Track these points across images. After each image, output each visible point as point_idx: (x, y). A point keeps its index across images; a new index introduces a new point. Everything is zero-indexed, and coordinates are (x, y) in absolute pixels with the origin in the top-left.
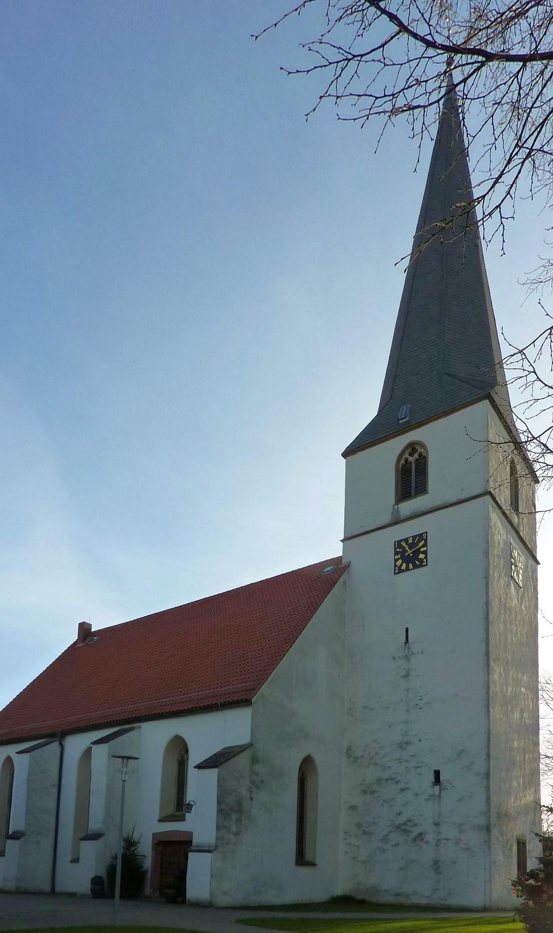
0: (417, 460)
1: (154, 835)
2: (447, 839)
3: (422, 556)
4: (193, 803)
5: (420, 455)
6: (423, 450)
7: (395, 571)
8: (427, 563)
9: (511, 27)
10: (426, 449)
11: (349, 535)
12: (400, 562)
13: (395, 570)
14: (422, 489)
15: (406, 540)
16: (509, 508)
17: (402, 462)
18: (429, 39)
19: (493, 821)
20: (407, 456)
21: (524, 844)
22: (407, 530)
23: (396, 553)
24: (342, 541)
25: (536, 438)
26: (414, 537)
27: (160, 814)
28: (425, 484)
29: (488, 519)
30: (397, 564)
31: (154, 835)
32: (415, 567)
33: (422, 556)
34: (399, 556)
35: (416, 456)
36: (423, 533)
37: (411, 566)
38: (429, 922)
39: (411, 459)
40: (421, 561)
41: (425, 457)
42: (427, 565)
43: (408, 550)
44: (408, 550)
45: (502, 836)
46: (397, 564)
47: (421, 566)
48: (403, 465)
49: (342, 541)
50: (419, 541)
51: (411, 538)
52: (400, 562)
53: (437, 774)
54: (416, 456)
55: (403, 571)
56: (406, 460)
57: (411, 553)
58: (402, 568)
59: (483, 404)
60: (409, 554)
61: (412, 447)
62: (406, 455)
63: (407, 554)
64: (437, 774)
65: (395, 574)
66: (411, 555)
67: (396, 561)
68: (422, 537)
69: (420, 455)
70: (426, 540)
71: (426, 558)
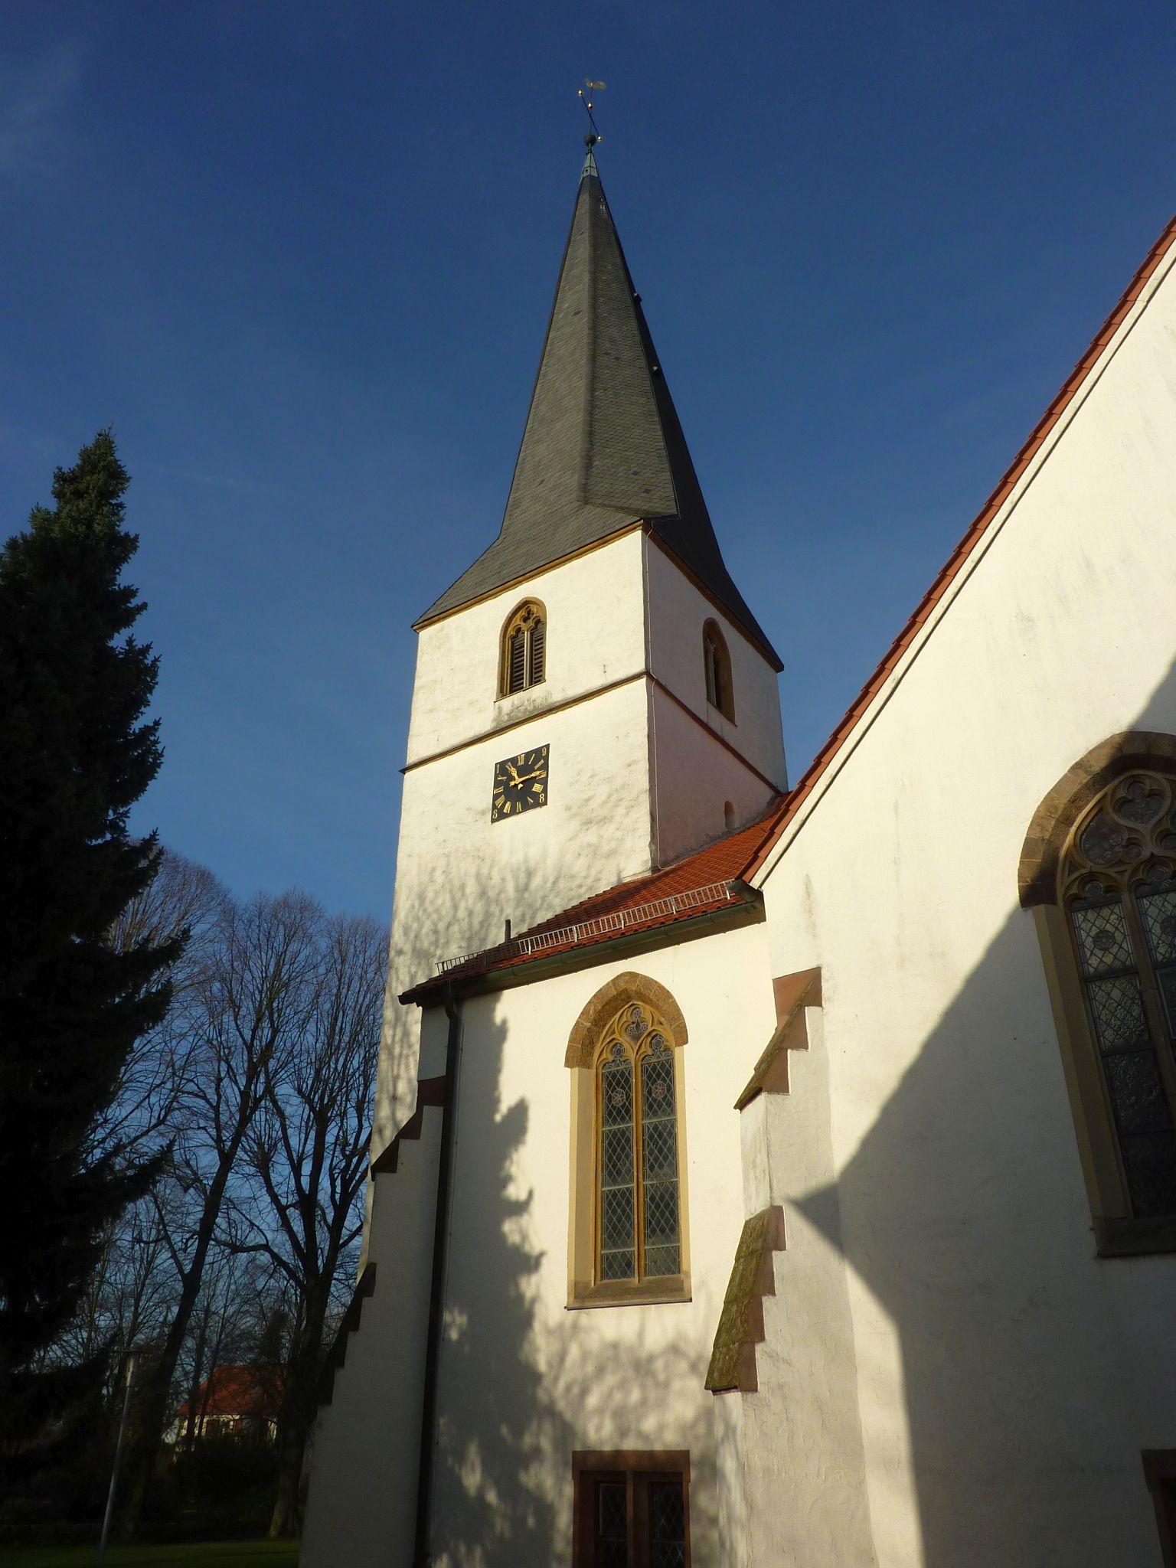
3: (537, 788)
9: (359, 1078)
12: (502, 798)
14: (537, 676)
15: (514, 761)
18: (346, 1223)
19: (206, 1273)
22: (517, 743)
23: (497, 785)
25: (1100, 988)
26: (528, 755)
28: (541, 671)
30: (497, 803)
32: (526, 807)
33: (537, 788)
34: (501, 789)
37: (519, 805)
38: (1083, 829)
40: (536, 795)
43: (516, 777)
44: (516, 777)
47: (538, 804)
50: (535, 762)
52: (502, 798)
57: (521, 783)
58: (505, 811)
59: (402, 1164)
60: (516, 785)
63: (512, 783)
66: (520, 786)
67: (496, 797)
68: (539, 757)
70: (546, 758)
71: (545, 791)
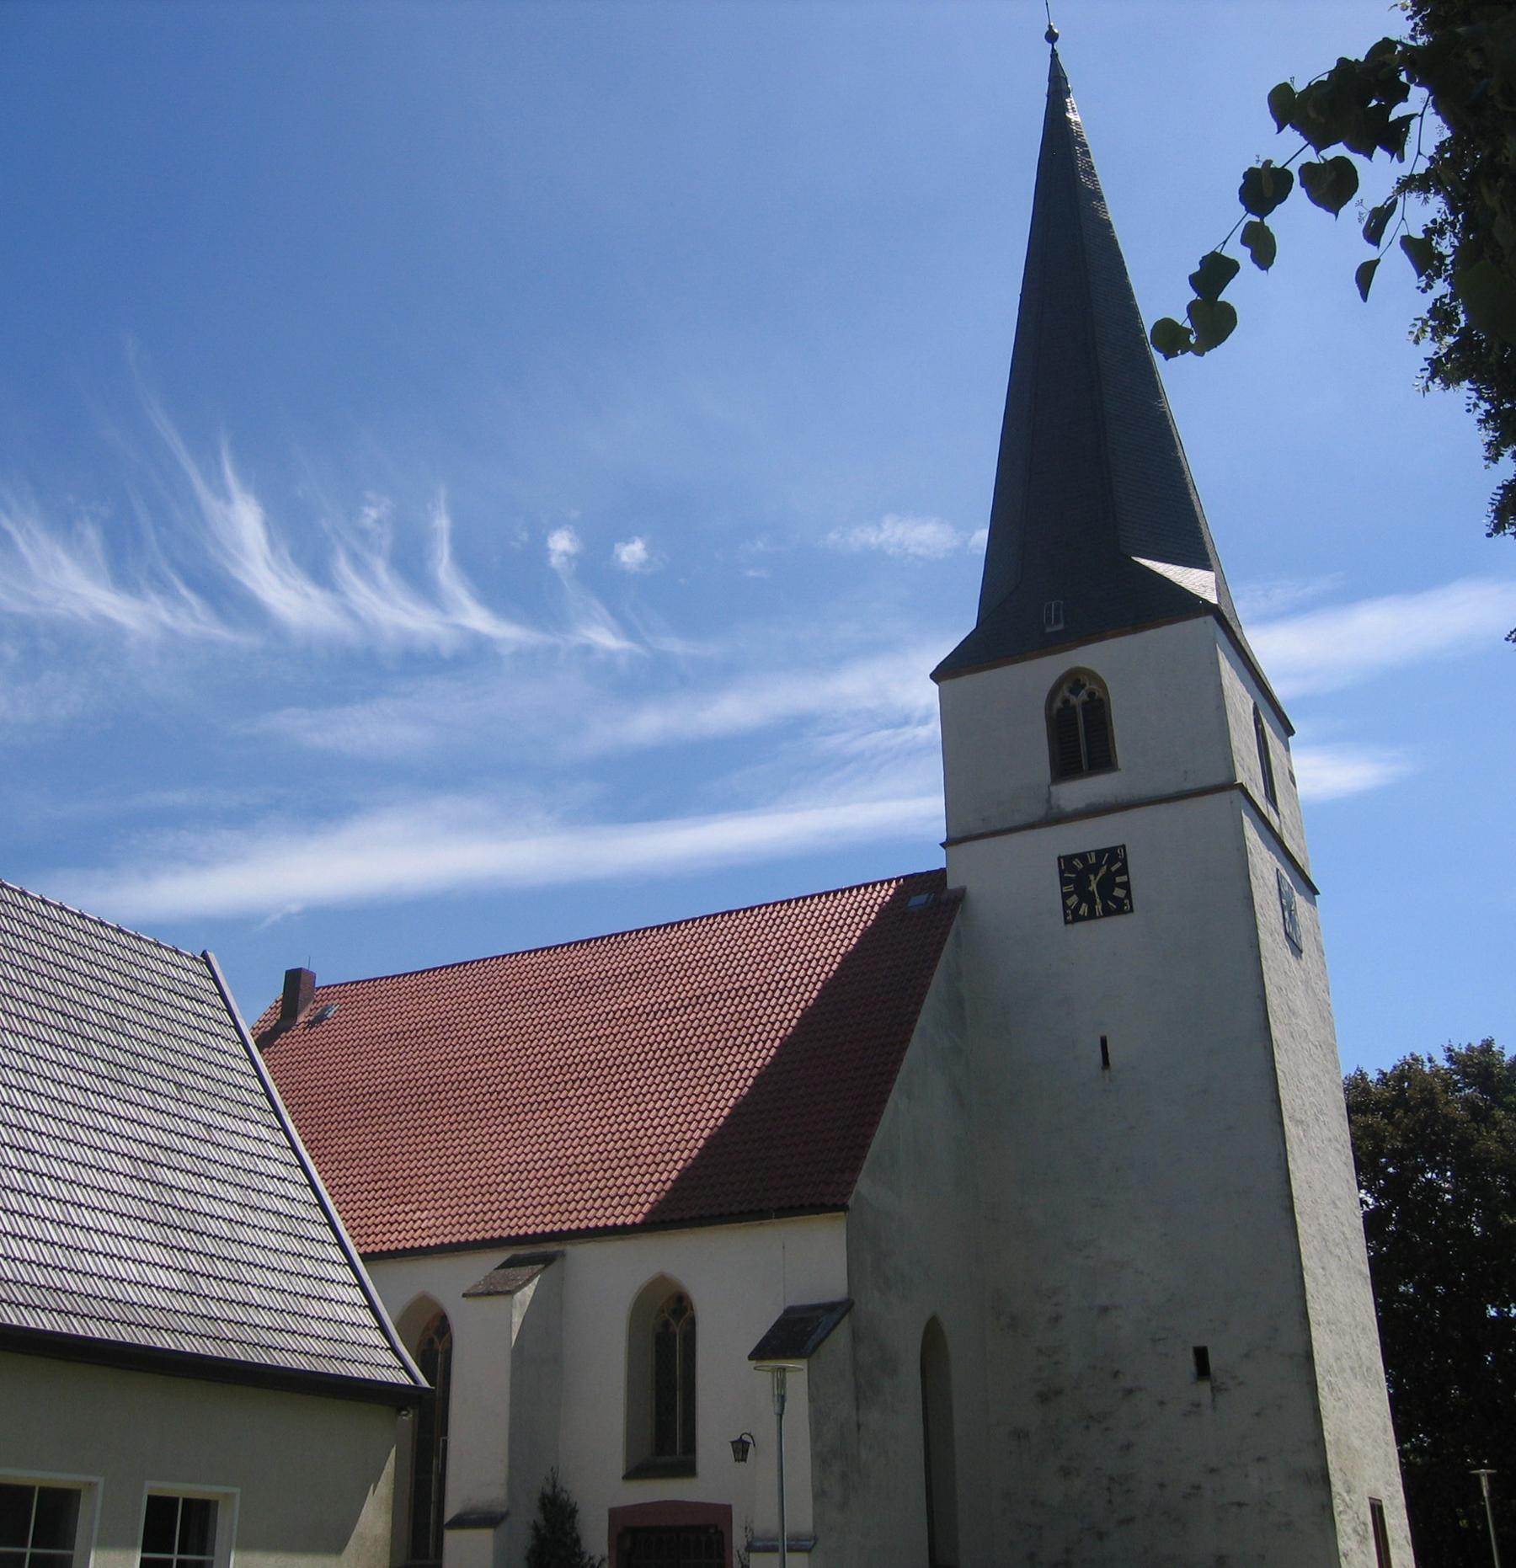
0: (1085, 704)
1: (614, 1514)
2: (1240, 1505)
4: (750, 1440)
5: (1091, 694)
6: (1094, 687)
7: (1065, 919)
8: (1131, 907)
10: (1104, 687)
11: (956, 834)
13: (1066, 915)
14: (1102, 759)
16: (1264, 801)
17: (1058, 704)
20: (1067, 694)
21: (1381, 1508)
23: (1064, 882)
24: (942, 845)
26: (1100, 853)
27: (628, 1460)
29: (1241, 831)
31: (614, 1514)
34: (1070, 888)
35: (1083, 695)
36: (1117, 847)
39: (1074, 700)
41: (1101, 700)
42: (1131, 910)
45: (1348, 1492)
46: (1069, 902)
48: (1059, 711)
49: (942, 845)
51: (1093, 854)
53: (1201, 1355)
54: (1083, 695)
55: (1083, 919)
56: (1066, 702)
58: (1081, 912)
61: (1075, 679)
62: (1065, 692)
64: (1201, 1355)
65: (1067, 922)
67: (1065, 896)
69: (1091, 694)
70: (1124, 862)
